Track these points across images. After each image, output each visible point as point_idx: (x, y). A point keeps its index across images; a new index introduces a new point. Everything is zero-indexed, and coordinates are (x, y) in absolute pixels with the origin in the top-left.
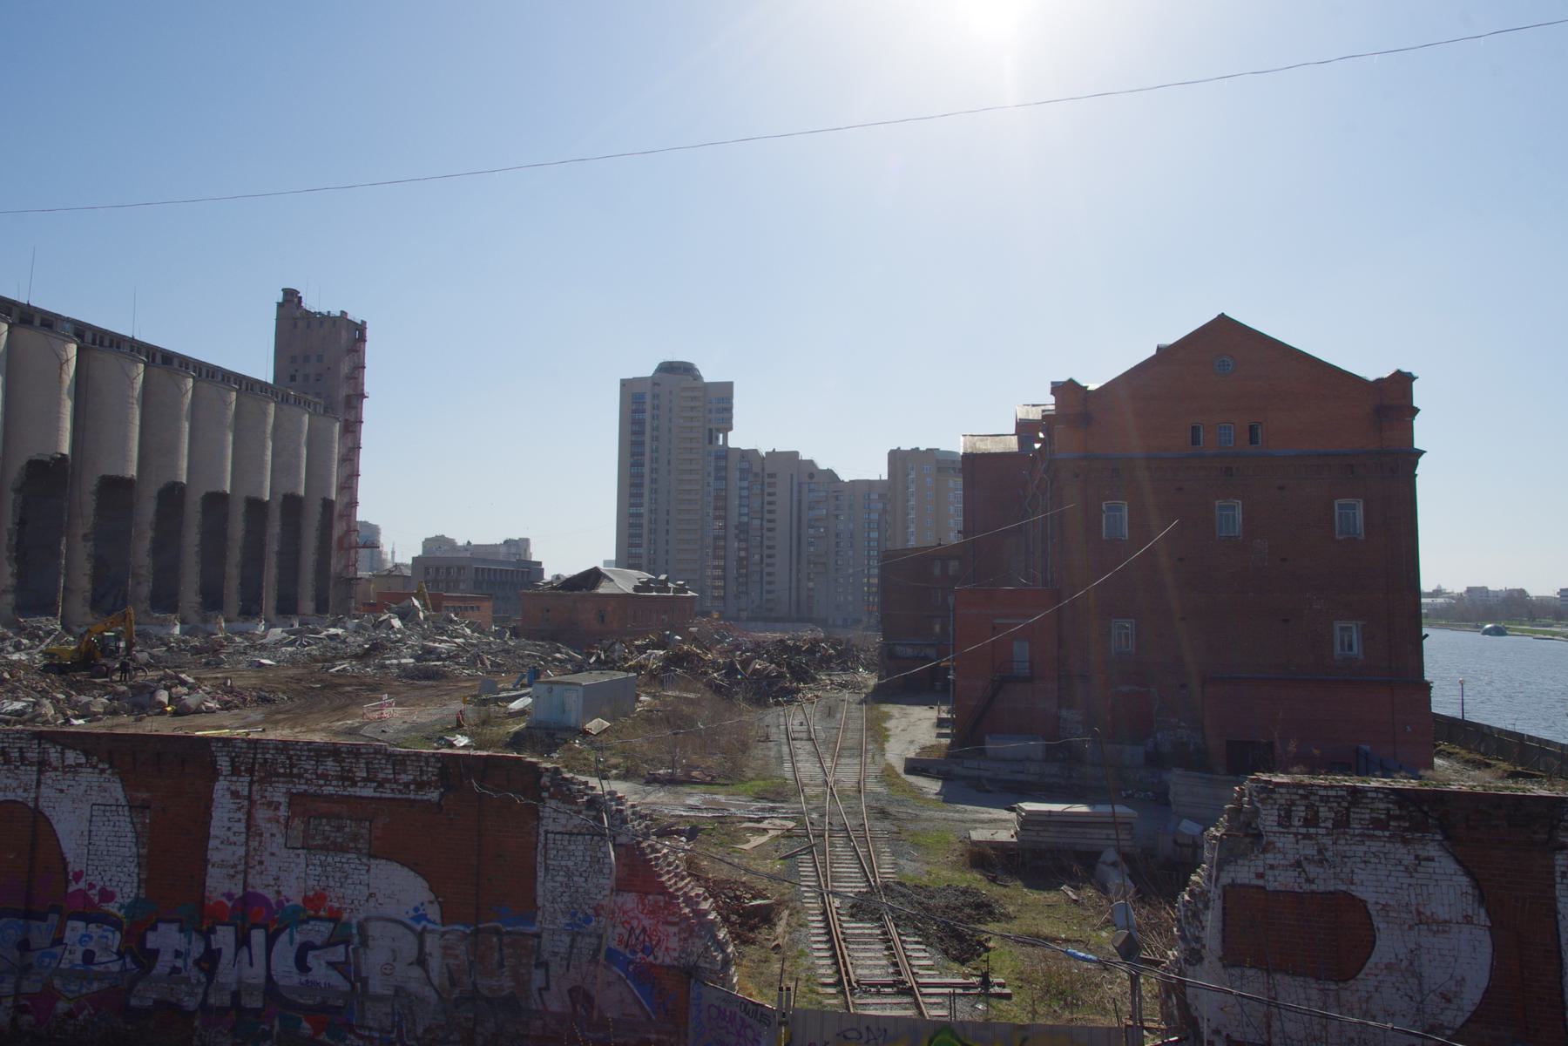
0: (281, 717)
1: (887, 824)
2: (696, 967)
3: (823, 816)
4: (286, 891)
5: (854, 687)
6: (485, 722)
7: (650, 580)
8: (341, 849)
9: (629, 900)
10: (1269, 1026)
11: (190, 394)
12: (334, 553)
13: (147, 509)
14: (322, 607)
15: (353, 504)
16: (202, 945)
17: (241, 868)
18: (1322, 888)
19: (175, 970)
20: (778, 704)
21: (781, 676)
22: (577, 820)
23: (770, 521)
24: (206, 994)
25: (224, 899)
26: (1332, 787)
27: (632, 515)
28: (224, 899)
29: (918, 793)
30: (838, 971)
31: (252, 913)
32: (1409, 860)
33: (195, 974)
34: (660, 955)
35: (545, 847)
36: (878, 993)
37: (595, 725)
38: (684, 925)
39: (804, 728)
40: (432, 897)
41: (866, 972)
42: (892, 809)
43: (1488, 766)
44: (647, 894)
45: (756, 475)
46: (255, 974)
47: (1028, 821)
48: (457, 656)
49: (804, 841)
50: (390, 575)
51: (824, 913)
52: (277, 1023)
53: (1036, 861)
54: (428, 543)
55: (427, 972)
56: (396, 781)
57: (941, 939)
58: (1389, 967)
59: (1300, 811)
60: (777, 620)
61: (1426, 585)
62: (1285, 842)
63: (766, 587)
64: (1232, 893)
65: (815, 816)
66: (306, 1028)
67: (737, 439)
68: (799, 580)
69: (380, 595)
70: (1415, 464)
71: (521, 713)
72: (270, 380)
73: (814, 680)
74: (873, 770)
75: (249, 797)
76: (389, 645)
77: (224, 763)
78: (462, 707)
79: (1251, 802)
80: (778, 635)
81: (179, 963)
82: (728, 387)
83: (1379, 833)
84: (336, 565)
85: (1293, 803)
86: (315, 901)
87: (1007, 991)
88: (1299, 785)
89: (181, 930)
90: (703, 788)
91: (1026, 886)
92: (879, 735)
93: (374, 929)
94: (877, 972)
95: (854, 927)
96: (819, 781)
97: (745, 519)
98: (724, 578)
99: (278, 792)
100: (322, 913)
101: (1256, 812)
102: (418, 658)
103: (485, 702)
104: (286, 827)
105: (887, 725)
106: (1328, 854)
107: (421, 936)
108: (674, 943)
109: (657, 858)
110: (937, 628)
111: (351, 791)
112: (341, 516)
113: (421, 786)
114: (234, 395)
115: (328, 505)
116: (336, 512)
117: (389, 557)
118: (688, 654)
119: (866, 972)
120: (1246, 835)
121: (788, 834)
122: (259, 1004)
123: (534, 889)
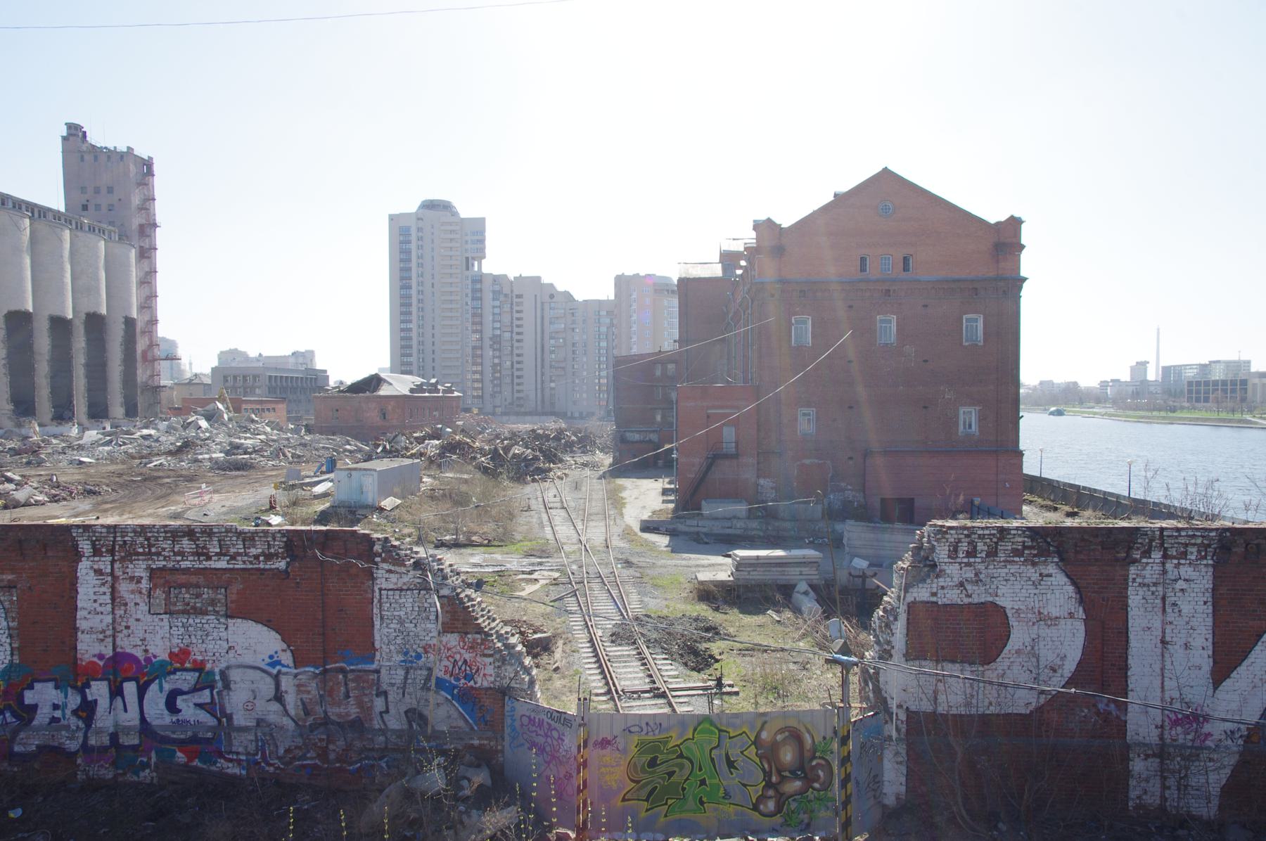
0: (109, 506)
1: (631, 571)
2: (509, 687)
3: (581, 567)
4: (152, 650)
5: (594, 466)
6: (295, 503)
7: (422, 384)
8: (204, 612)
9: (452, 639)
10: (936, 699)
11: (28, 230)
12: (139, 365)
14: (131, 411)
15: (153, 322)
16: (79, 699)
17: (109, 633)
18: (976, 601)
19: (54, 720)
20: (534, 481)
21: (536, 458)
22: (405, 579)
23: (518, 334)
24: (86, 737)
25: (95, 659)
26: (987, 528)
27: (402, 330)
28: (95, 659)
29: (652, 547)
30: (607, 684)
31: (122, 669)
32: (1035, 577)
33: (74, 722)
34: (479, 680)
35: (380, 601)
36: (639, 698)
37: (389, 503)
38: (498, 656)
39: (558, 499)
40: (285, 646)
41: (628, 683)
42: (634, 560)
43: (1056, 509)
44: (466, 633)
45: (506, 295)
46: (131, 718)
47: (741, 565)
48: (261, 450)
49: (570, 588)
50: (190, 383)
51: (591, 641)
52: (153, 755)
53: (744, 595)
54: (222, 356)
55: (284, 706)
56: (246, 554)
57: (682, 655)
58: (1018, 652)
59: (964, 547)
60: (526, 414)
61: (1128, 379)
62: (953, 570)
63: (516, 388)
64: (911, 607)
65: (574, 567)
66: (181, 757)
67: (491, 265)
68: (543, 382)
69: (184, 400)
70: (1020, 288)
71: (325, 495)
72: (62, 209)
73: (561, 461)
74: (616, 530)
75: (112, 574)
76: (199, 442)
77: (85, 546)
78: (274, 492)
79: (929, 542)
80: (529, 427)
81: (58, 714)
82: (481, 222)
83: (1017, 559)
84: (142, 375)
85: (960, 541)
86: (180, 657)
87: (735, 689)
88: (965, 528)
89: (57, 687)
90: (482, 549)
91: (743, 612)
92: (617, 502)
93: (234, 675)
94: (637, 682)
95: (614, 650)
96: (575, 541)
97: (498, 332)
98: (482, 381)
99: (139, 568)
100: (187, 665)
101: (933, 549)
102: (227, 453)
103: (293, 487)
104: (149, 596)
105: (623, 495)
106: (982, 576)
107: (276, 678)
108: (490, 670)
109: (473, 606)
110: (659, 418)
111: (207, 564)
112: (143, 332)
113: (269, 557)
114: (27, 221)
115: (130, 323)
116: (138, 330)
117: (187, 368)
118: (459, 443)
119: (628, 683)
120: (925, 566)
121: (555, 582)
122: (136, 742)
123: (372, 635)
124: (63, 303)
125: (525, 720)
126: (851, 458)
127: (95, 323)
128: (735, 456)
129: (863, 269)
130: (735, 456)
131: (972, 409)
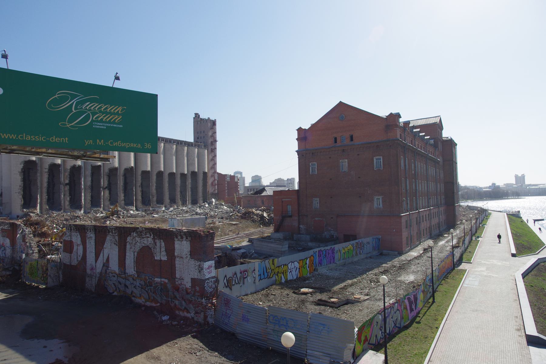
13: (154, 178)
124: (184, 169)
126: (332, 218)
127: (194, 174)
128: (291, 216)
129: (336, 142)
130: (291, 216)
131: (380, 197)
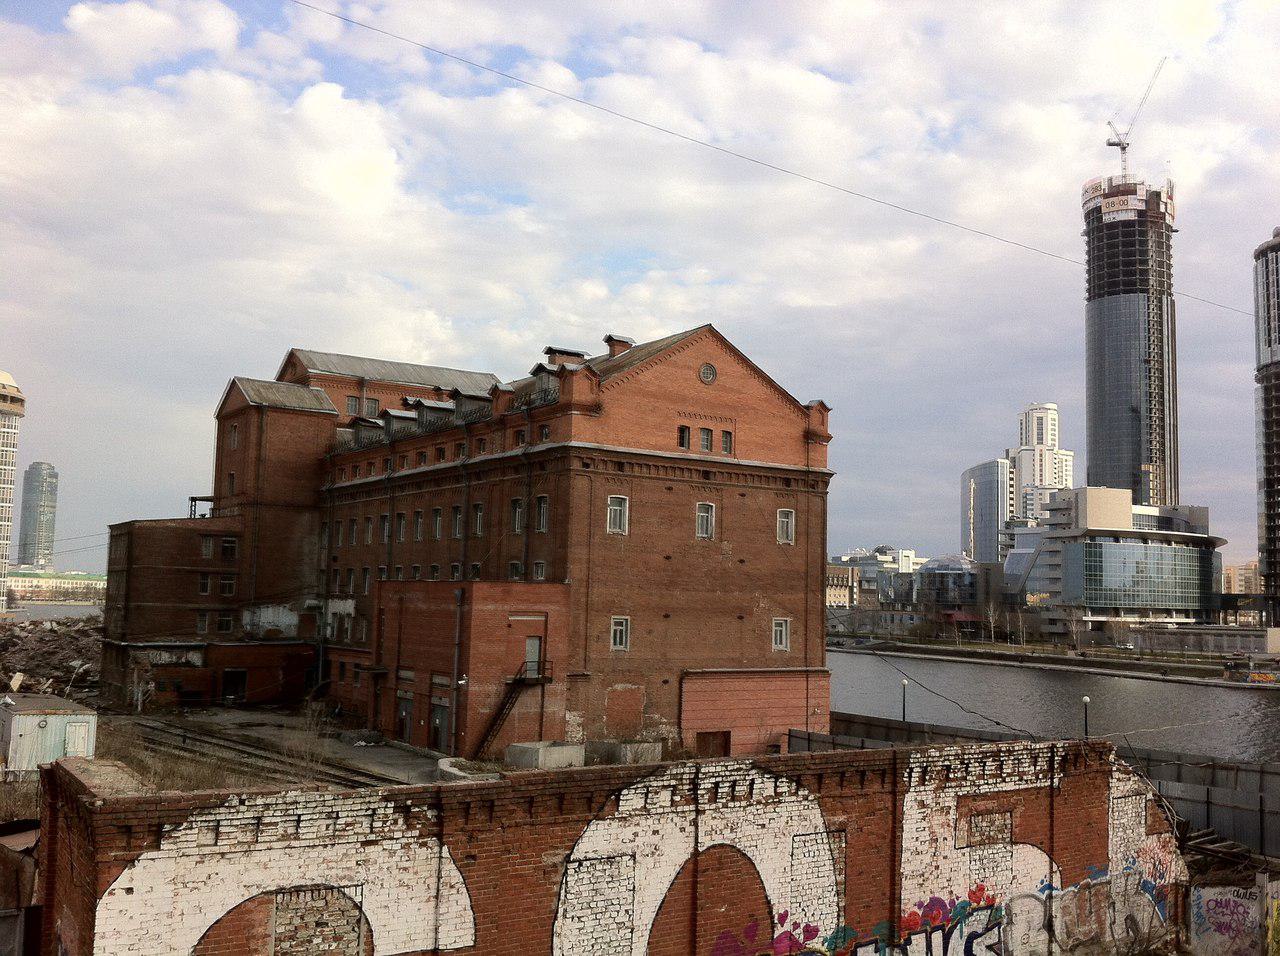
125: (1212, 905)
126: (666, 682)
